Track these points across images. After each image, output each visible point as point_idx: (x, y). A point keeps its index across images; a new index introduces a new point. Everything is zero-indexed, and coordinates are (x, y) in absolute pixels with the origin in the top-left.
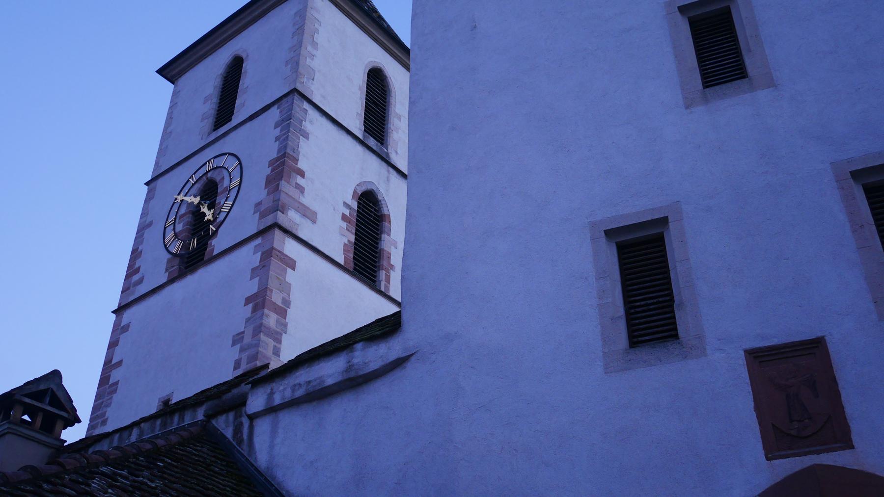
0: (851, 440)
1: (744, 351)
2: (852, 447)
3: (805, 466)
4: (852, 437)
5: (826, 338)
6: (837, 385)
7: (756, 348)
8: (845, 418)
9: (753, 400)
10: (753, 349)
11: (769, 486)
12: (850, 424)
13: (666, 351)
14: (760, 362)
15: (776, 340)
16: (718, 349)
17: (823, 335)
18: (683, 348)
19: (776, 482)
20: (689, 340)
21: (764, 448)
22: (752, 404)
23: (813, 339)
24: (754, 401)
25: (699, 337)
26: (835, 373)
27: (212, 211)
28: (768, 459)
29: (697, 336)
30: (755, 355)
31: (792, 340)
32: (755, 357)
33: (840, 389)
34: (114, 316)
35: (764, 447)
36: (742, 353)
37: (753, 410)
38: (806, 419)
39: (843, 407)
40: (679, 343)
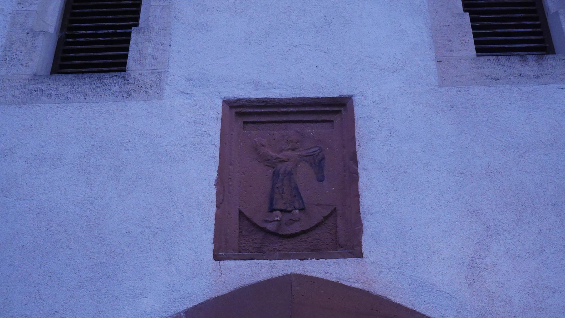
0: (360, 244)
1: (224, 101)
2: (360, 255)
3: (275, 275)
4: (363, 240)
5: (354, 98)
6: (356, 162)
7: (243, 99)
8: (358, 212)
9: (217, 169)
10: (238, 100)
11: (247, 97)
12: (365, 223)
13: (100, 85)
14: (245, 123)
15: (277, 91)
16: (183, 93)
17: (351, 94)
18: (128, 84)
19: (221, 294)
20: (141, 74)
21: (216, 240)
22: (214, 174)
23: (334, 98)
24: (218, 171)
25: (159, 73)
26: (357, 147)
27: (278, 217)
28: (216, 257)
29: (155, 71)
30: (238, 110)
31: (302, 96)
32: (239, 114)
33: (359, 171)
34: (322, 218)
35: (215, 238)
36: (220, 103)
37: (213, 182)
38: (295, 209)
39: (358, 196)
40: (124, 77)
